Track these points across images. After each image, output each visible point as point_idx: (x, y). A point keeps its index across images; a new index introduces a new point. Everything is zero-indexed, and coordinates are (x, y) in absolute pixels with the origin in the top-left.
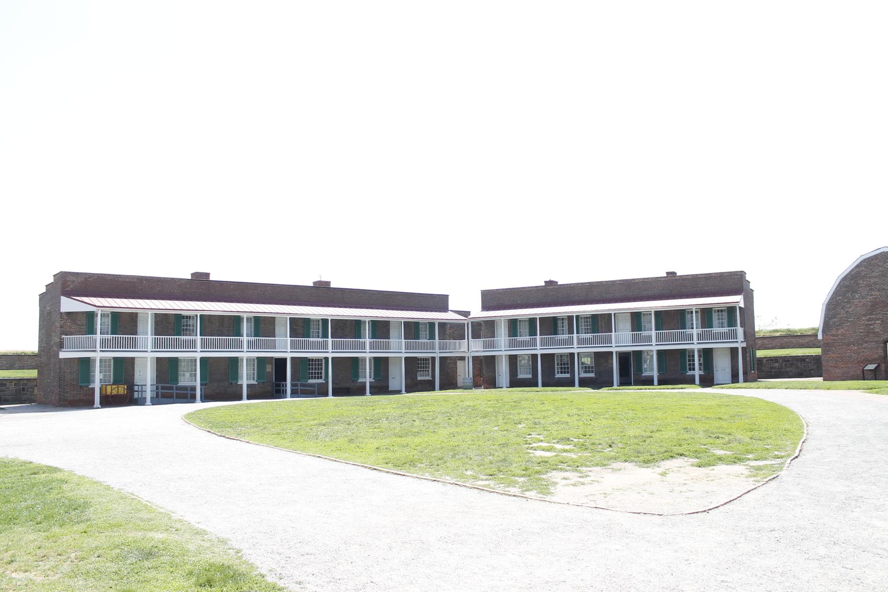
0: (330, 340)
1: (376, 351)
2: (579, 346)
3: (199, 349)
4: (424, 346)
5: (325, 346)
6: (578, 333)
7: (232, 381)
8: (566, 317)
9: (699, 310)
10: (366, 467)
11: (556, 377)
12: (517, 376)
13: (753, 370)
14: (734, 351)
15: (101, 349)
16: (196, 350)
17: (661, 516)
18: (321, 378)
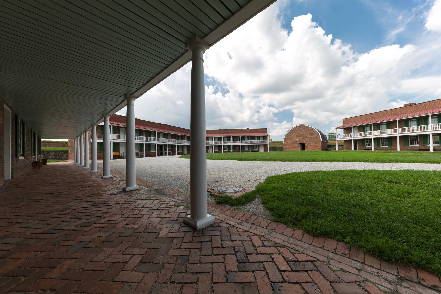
6: (168, 138)
8: (344, 141)
11: (151, 151)
12: (150, 151)
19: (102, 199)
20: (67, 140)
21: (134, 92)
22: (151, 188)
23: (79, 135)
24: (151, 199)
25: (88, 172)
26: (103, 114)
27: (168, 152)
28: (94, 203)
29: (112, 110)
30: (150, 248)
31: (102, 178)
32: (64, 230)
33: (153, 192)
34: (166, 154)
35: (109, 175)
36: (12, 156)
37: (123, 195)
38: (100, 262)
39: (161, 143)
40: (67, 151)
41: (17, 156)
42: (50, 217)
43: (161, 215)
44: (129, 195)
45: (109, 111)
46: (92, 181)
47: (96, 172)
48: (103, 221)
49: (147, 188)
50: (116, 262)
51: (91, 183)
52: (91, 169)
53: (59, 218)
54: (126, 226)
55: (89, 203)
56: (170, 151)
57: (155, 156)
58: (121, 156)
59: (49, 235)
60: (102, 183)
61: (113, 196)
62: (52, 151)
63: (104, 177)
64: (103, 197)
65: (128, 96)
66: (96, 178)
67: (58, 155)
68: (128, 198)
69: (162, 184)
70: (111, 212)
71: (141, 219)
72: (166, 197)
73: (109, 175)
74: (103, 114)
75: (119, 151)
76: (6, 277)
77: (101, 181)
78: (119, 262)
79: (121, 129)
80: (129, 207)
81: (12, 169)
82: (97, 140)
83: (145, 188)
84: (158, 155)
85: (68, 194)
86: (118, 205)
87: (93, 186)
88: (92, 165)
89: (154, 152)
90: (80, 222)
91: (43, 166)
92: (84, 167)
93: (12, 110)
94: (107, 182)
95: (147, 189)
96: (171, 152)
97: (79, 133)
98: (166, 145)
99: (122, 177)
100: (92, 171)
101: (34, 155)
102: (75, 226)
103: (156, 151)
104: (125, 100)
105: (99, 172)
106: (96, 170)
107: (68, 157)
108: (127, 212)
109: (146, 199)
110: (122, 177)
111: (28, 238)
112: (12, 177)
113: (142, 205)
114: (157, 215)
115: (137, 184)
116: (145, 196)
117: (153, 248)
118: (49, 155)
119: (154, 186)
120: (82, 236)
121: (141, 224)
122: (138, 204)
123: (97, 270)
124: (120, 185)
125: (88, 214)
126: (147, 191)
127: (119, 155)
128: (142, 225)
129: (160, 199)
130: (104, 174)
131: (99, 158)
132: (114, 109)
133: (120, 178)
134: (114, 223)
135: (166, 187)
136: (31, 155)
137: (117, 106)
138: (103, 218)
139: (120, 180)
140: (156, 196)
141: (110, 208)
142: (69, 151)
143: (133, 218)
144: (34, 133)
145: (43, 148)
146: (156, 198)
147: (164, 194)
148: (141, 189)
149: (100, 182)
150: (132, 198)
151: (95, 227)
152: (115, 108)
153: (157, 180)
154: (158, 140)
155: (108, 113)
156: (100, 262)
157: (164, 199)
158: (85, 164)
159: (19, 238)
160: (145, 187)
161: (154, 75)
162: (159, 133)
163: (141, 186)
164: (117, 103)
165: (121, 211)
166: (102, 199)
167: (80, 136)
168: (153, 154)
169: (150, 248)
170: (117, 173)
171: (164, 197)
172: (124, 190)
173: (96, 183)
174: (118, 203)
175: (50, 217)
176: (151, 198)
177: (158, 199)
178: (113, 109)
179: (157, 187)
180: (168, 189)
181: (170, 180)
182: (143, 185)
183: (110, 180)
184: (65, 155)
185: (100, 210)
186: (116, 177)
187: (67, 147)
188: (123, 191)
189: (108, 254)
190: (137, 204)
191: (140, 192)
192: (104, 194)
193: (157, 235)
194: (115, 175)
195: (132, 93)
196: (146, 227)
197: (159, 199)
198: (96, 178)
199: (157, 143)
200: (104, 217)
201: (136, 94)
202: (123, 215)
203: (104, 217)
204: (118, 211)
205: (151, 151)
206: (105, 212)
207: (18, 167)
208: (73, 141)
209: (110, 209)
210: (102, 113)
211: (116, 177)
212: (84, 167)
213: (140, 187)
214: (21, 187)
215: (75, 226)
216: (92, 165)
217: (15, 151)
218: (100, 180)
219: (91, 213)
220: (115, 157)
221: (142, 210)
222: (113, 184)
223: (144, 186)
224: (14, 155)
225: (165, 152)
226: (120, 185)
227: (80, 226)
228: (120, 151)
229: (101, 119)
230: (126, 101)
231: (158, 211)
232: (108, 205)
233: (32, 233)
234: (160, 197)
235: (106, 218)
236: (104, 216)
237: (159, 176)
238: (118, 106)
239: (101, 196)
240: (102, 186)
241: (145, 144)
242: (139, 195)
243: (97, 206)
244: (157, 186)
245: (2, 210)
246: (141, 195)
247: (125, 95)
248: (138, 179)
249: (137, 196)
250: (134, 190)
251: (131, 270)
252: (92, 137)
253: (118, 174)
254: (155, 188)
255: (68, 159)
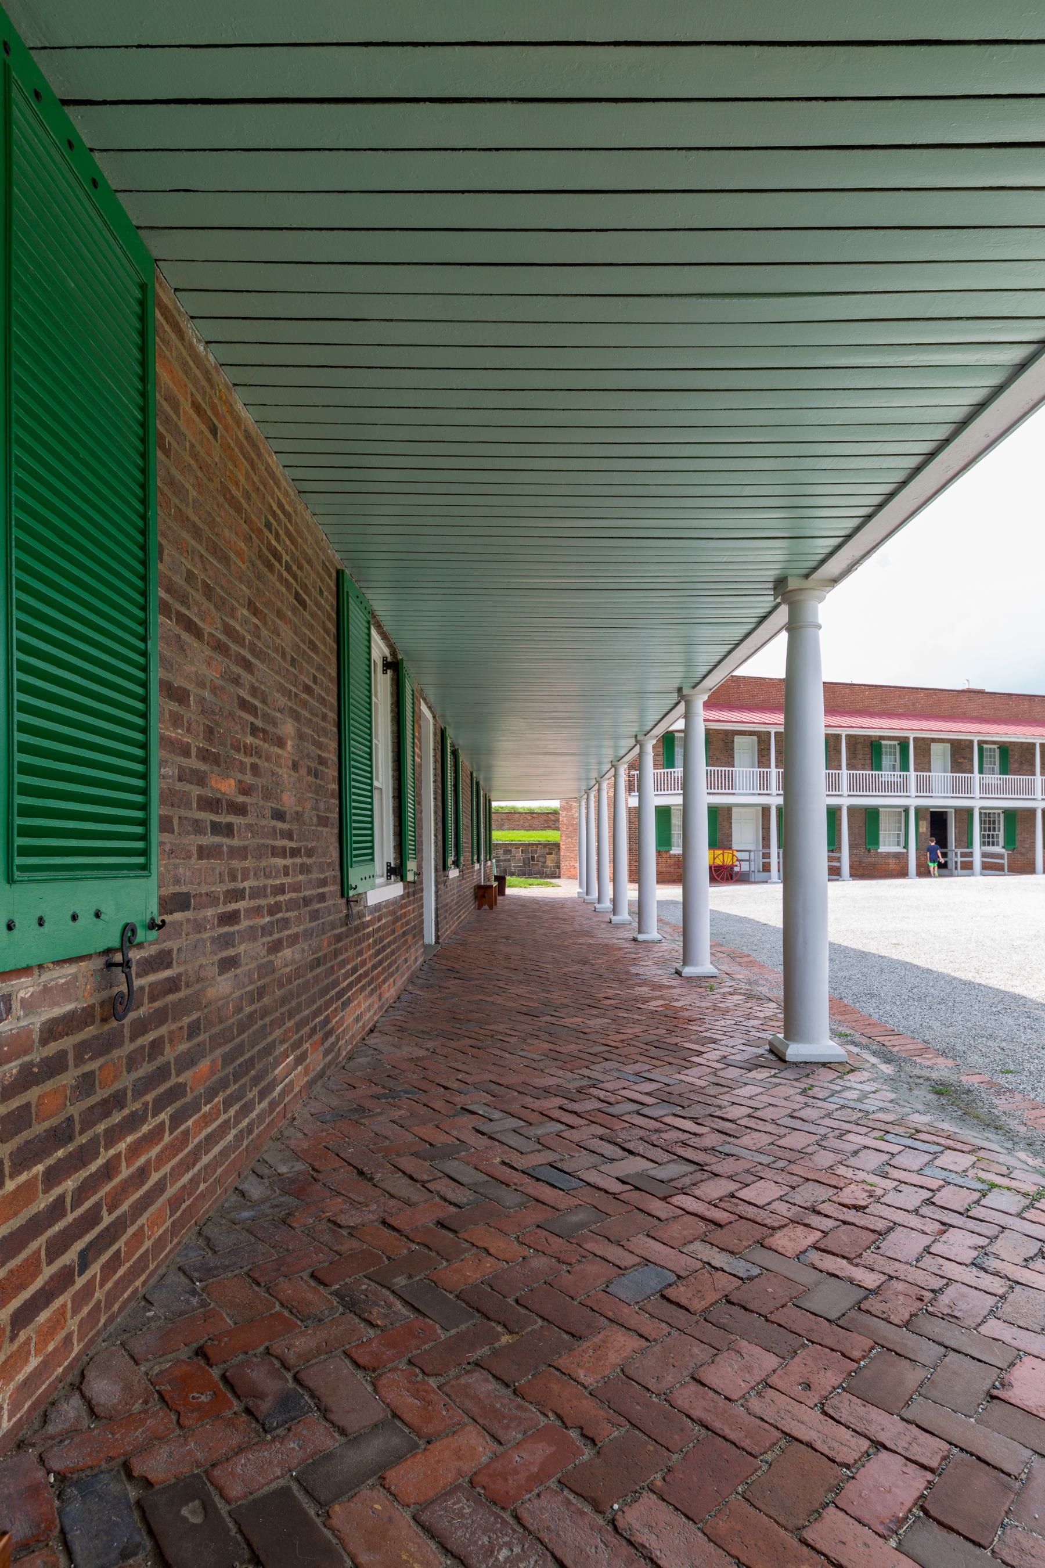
0: (844, 772)
1: (858, 793)
2: (831, 793)
3: (845, 792)
4: (891, 787)
5: (904, 787)
6: (981, 772)
7: (165, 917)
9: (995, 746)
10: (558, 1370)
11: (882, 849)
12: (877, 843)
13: (456, 863)
14: (766, 810)
15: (709, 791)
16: (768, 792)
17: (978, 1551)
18: (998, 845)
19: (692, 1077)
20: (555, 804)
21: (820, 557)
22: (908, 1068)
23: (593, 782)
24: (922, 1136)
25: (626, 939)
26: (680, 690)
27: (984, 855)
28: (668, 1089)
29: (715, 666)
30: (962, 1450)
31: (678, 973)
32: (588, 1184)
33: (923, 1094)
34: (968, 866)
35: (704, 966)
36: (436, 870)
37: (774, 1076)
38: (729, 1400)
39: (941, 799)
40: (557, 846)
41: (445, 868)
42: (542, 1113)
43: (997, 1257)
44: (803, 1086)
45: (704, 670)
46: (644, 983)
47: (653, 942)
48: (715, 1189)
49: (888, 1061)
50: (801, 1442)
51: (643, 991)
52: (636, 925)
53: (567, 1125)
54: (814, 1256)
55: (649, 1087)
56: (998, 849)
57: (903, 873)
58: (736, 869)
59: (548, 1190)
60: (685, 999)
61: (733, 1073)
62: (517, 846)
63: (688, 971)
64: (695, 1071)
65: (793, 584)
66: (659, 972)
67: (533, 858)
68: (802, 1099)
69: (974, 1058)
70: (738, 1158)
71: (888, 1245)
72: (1009, 1145)
73: (704, 966)
74: (680, 690)
75: (730, 848)
76: (464, 1305)
77: (678, 991)
78: (809, 1445)
79: (738, 739)
80: (809, 1150)
81: (437, 909)
82: (656, 800)
83: (874, 1060)
84: (923, 872)
85: (578, 1028)
86: (761, 1125)
87: (653, 1005)
88: (640, 909)
89: (897, 855)
90: (633, 1166)
91: (500, 898)
92: (612, 917)
93: (434, 717)
94: (702, 997)
95: (887, 1069)
96: (1000, 856)
97: (594, 774)
98: (969, 811)
99: (756, 983)
100: (641, 937)
101: (479, 861)
102: (617, 1179)
103: (906, 847)
104: (776, 607)
105: (666, 946)
106: (653, 933)
107: (559, 867)
108: (808, 1180)
109: (889, 1128)
110: (756, 983)
111: (497, 1180)
112: (437, 942)
113: (873, 1160)
114: (975, 1254)
115: (835, 1034)
116: (882, 1109)
117: (979, 1458)
118: (509, 860)
119: (929, 1063)
120: (648, 1236)
121: (891, 1277)
122: (855, 1147)
123: (724, 1438)
124: (756, 1022)
125: (654, 1137)
126: (889, 1080)
127: (732, 867)
128: (894, 1282)
129: (975, 1150)
130: (686, 960)
131: (663, 878)
132: (725, 657)
133: (750, 984)
134: (759, 1220)
135: (1001, 1080)
136: (473, 863)
137: (737, 645)
138: (709, 1178)
139: (749, 997)
140: (946, 1126)
141: (730, 1135)
142: (562, 847)
143: (844, 1223)
144: (478, 784)
145: (499, 836)
146: (948, 1137)
147: (1009, 1135)
148: (857, 1065)
149: (674, 991)
150: (820, 1104)
151: (688, 1213)
152: (730, 652)
153: (936, 1025)
154: (923, 786)
155: (701, 681)
156: (729, 1400)
157: (1002, 1159)
158: (615, 901)
159: (476, 1168)
160: (874, 1053)
161: (942, 433)
162: (924, 746)
163: (853, 1043)
164: (740, 631)
165: (781, 1164)
166: (692, 1077)
167: (596, 787)
168: (892, 864)
169: (962, 1450)
170: (734, 957)
171: (995, 1147)
172: (777, 1055)
173: (661, 997)
174: (758, 1114)
175: (542, 1113)
176: (918, 1131)
177: (959, 1146)
178: (720, 662)
179: (942, 1069)
180: (1018, 1097)
181: (1023, 1039)
182: (864, 1041)
183: (711, 989)
184: (550, 861)
185: (695, 1134)
186: (733, 979)
187: (557, 829)
188: (771, 1057)
189: (758, 1379)
190: (849, 1148)
191: (852, 1079)
192: (700, 1054)
193: (994, 1387)
194: (724, 967)
195: (813, 564)
196: (920, 1305)
197: (966, 1148)
198: (659, 972)
199: (913, 802)
200: (716, 1175)
201: (833, 566)
202: (793, 1188)
203: (716, 1175)
204: (765, 1160)
205: (882, 849)
206: (713, 1149)
207: (447, 904)
208: (575, 804)
209: (731, 1139)
210: (677, 685)
211: (733, 979)
212: (612, 917)
213: (849, 1052)
214: (458, 975)
215: (617, 1179)
216: (640, 909)
217: (441, 850)
218: (674, 983)
219: (664, 1135)
220: (721, 874)
221: (879, 1192)
222: (725, 1012)
223: (866, 1047)
224: (440, 867)
225: (963, 855)
226: (756, 1022)
227: (637, 1188)
228: (735, 847)
229: (671, 710)
230: (784, 609)
231: (977, 1229)
232: (718, 1113)
233: (504, 1163)
234: (971, 1135)
235: (723, 1182)
236: (715, 1168)
237: (943, 1001)
238: (742, 641)
239: (688, 1065)
240: (686, 1014)
241: (851, 809)
242: (847, 1094)
243: (678, 1110)
244: (940, 1060)
245: (428, 1050)
246: (859, 1100)
247: (780, 584)
248: (838, 1008)
249: (842, 1102)
250: (824, 1065)
251: (881, 1529)
252: (636, 785)
253: (740, 964)
254: (935, 1075)
255: (559, 877)
